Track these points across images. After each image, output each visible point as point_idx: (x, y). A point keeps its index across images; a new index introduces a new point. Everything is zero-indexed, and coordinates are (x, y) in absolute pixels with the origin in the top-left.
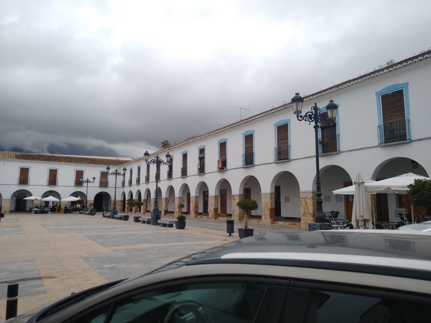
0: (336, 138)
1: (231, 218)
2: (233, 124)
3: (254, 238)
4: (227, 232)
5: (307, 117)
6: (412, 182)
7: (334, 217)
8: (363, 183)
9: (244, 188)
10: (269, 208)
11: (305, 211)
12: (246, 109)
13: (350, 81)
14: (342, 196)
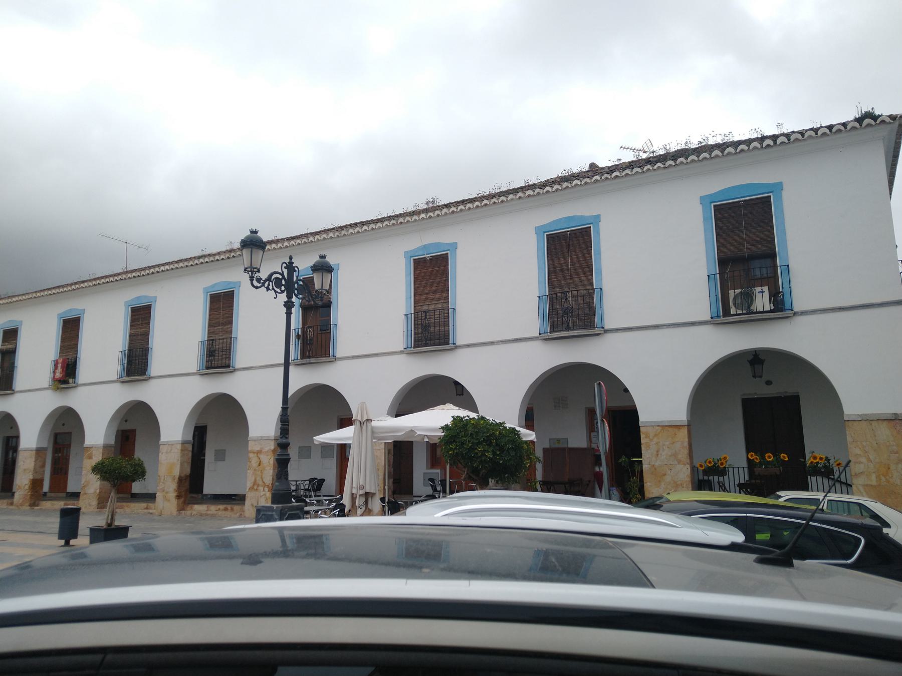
0: (329, 331)
1: (76, 502)
2: (102, 278)
3: (127, 546)
4: (60, 538)
5: (271, 283)
6: (448, 421)
7: (315, 491)
8: (369, 420)
9: (118, 431)
10: (175, 475)
11: (255, 480)
12: (140, 247)
13: (362, 223)
14: (334, 446)
